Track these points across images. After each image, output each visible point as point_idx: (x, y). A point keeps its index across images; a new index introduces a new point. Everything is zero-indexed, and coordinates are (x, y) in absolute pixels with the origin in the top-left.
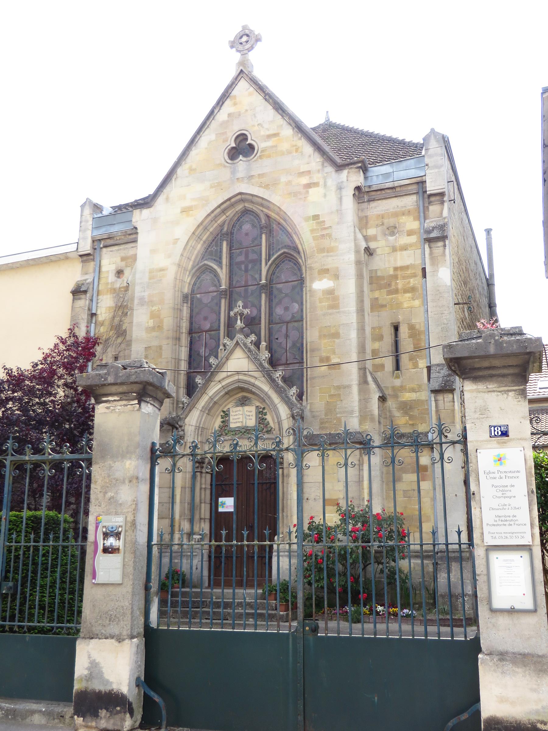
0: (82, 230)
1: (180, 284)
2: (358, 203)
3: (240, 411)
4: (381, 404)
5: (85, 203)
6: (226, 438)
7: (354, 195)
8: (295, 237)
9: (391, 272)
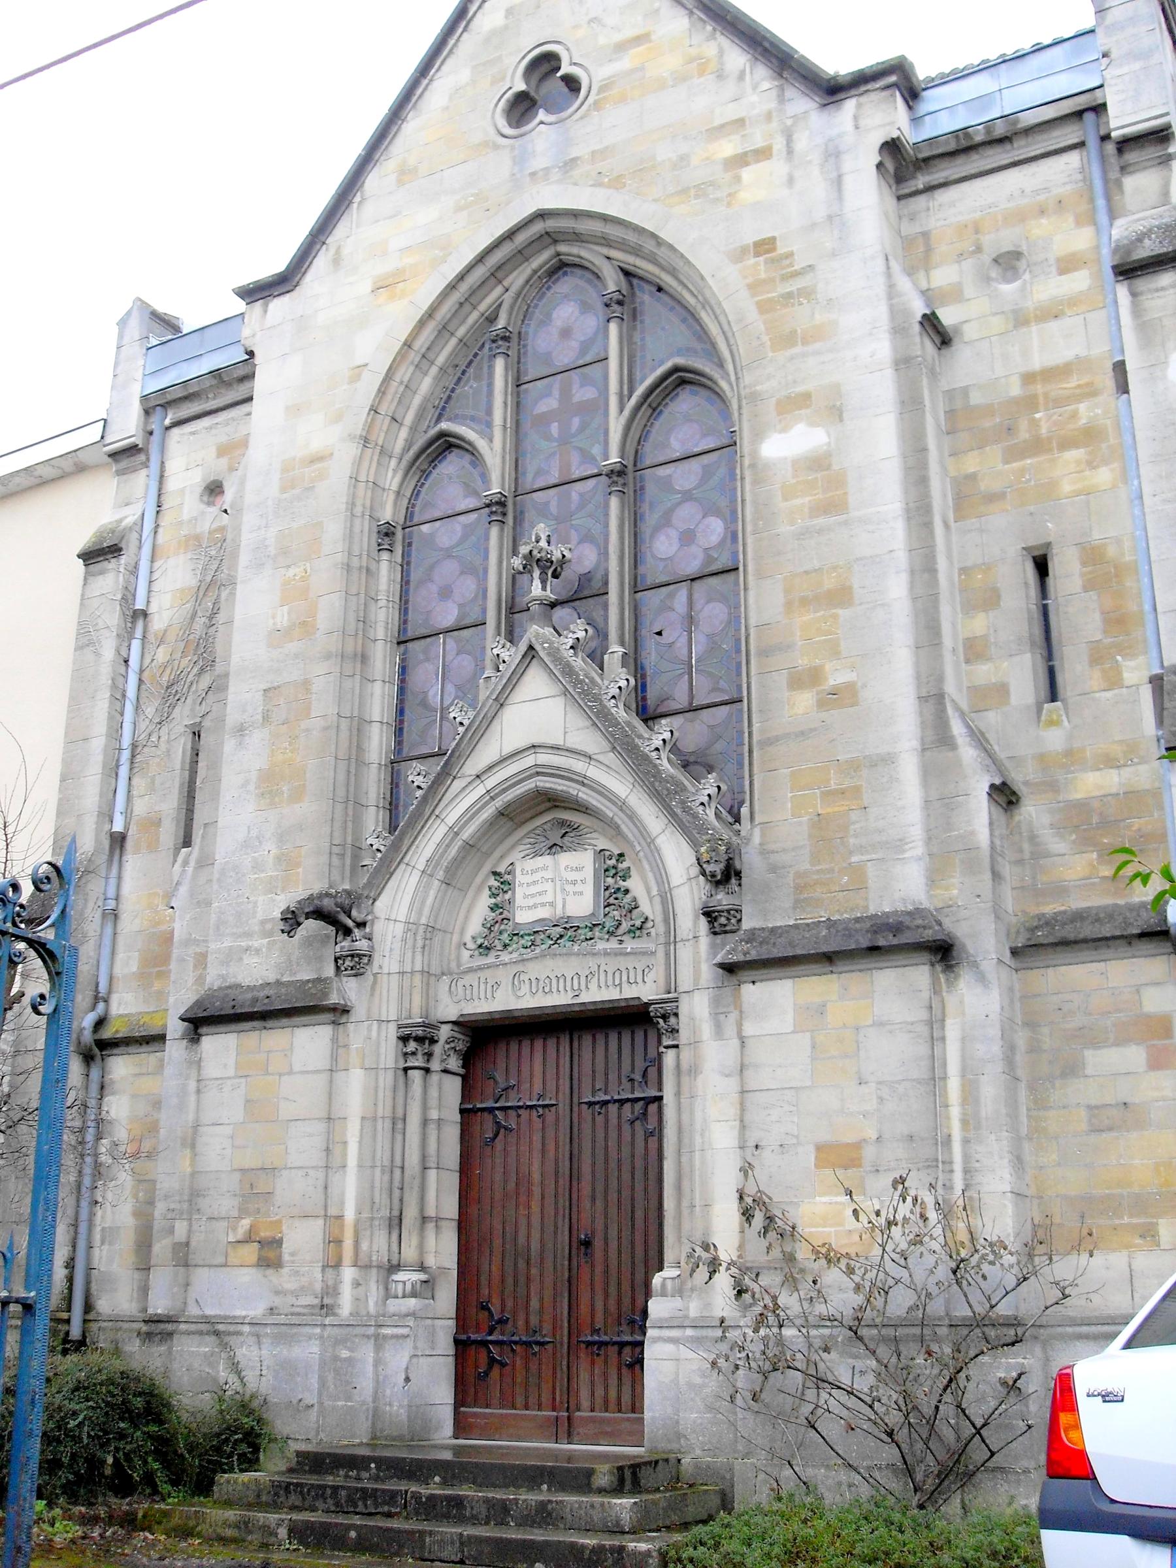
0: (118, 381)
1: (369, 493)
2: (899, 198)
3: (545, 868)
4: (998, 813)
6: (505, 957)
7: (880, 166)
8: (705, 316)
9: (1016, 390)
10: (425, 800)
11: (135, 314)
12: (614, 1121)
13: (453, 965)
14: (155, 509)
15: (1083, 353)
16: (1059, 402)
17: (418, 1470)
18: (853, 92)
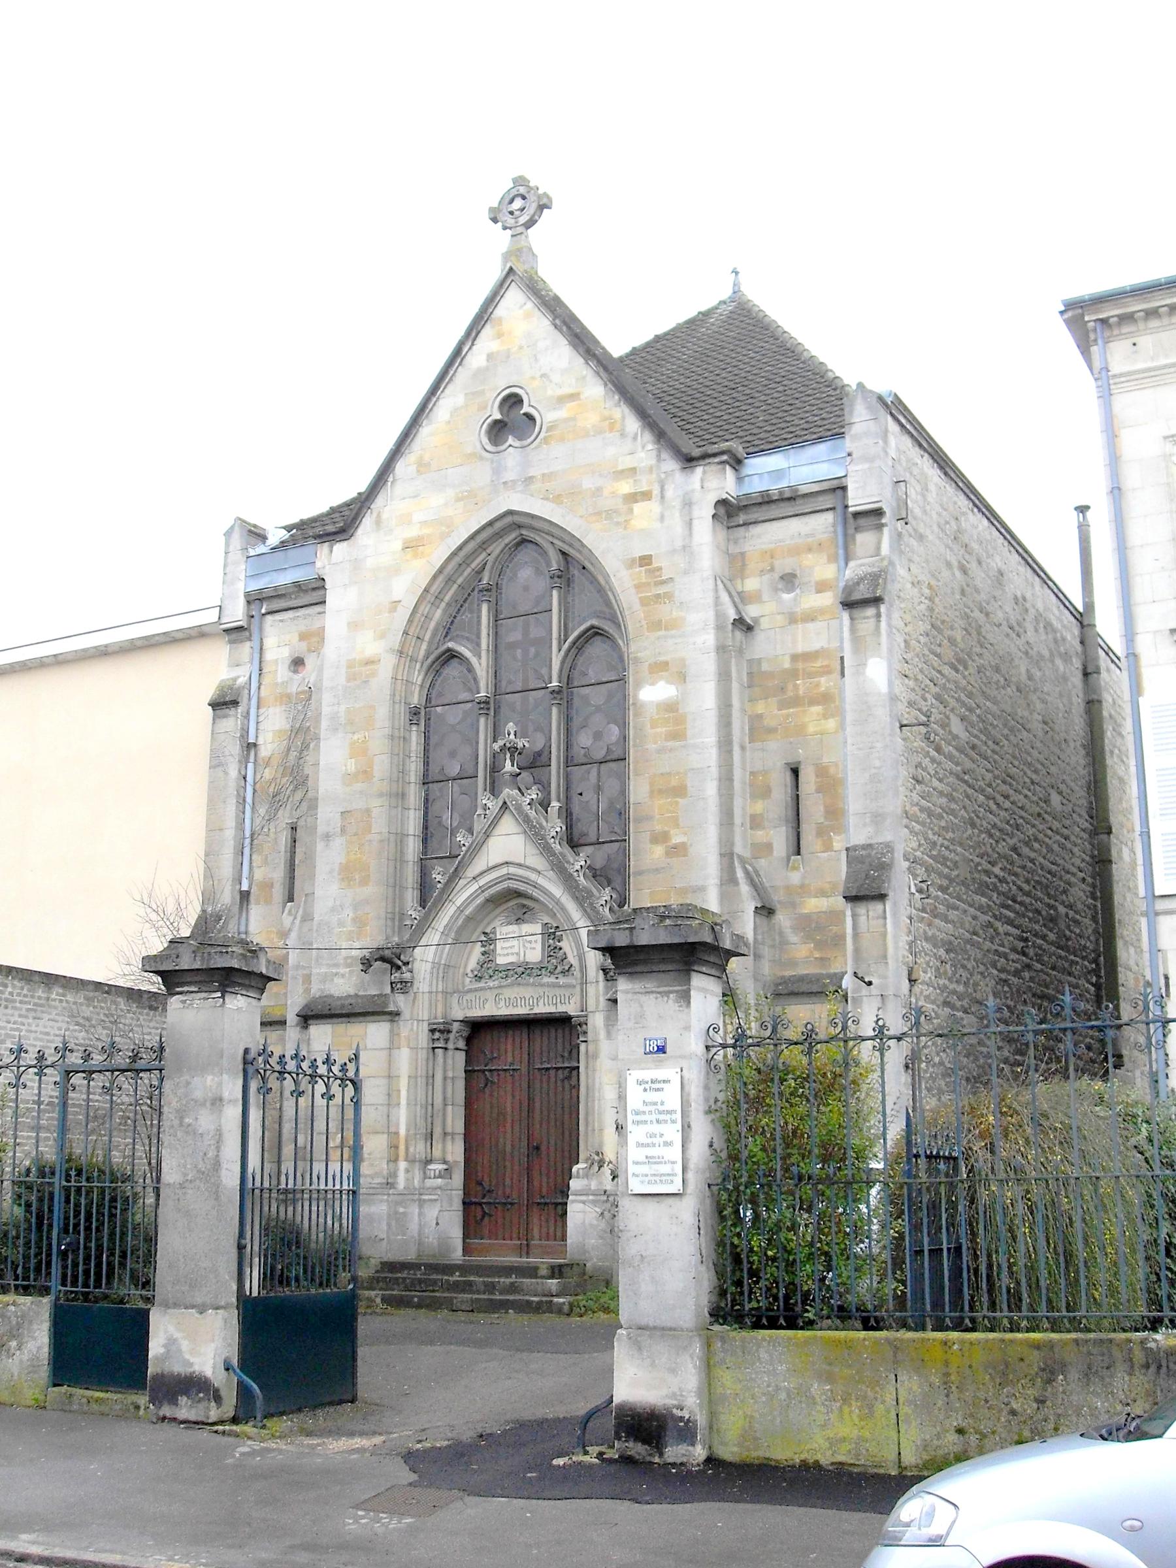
0: (227, 579)
5: (232, 528)
6: (491, 984)
10: (443, 890)
11: (237, 528)
12: (553, 1080)
13: (460, 987)
14: (258, 672)
15: (826, 646)
16: (810, 675)
17: (449, 1269)
18: (702, 462)
